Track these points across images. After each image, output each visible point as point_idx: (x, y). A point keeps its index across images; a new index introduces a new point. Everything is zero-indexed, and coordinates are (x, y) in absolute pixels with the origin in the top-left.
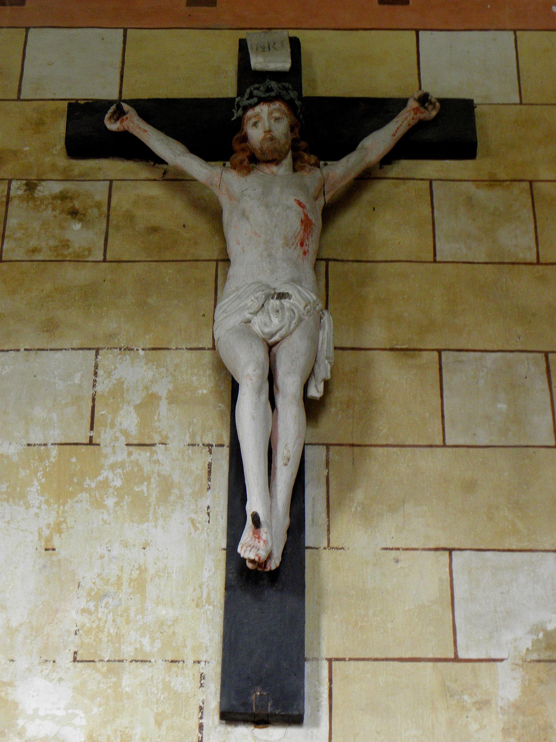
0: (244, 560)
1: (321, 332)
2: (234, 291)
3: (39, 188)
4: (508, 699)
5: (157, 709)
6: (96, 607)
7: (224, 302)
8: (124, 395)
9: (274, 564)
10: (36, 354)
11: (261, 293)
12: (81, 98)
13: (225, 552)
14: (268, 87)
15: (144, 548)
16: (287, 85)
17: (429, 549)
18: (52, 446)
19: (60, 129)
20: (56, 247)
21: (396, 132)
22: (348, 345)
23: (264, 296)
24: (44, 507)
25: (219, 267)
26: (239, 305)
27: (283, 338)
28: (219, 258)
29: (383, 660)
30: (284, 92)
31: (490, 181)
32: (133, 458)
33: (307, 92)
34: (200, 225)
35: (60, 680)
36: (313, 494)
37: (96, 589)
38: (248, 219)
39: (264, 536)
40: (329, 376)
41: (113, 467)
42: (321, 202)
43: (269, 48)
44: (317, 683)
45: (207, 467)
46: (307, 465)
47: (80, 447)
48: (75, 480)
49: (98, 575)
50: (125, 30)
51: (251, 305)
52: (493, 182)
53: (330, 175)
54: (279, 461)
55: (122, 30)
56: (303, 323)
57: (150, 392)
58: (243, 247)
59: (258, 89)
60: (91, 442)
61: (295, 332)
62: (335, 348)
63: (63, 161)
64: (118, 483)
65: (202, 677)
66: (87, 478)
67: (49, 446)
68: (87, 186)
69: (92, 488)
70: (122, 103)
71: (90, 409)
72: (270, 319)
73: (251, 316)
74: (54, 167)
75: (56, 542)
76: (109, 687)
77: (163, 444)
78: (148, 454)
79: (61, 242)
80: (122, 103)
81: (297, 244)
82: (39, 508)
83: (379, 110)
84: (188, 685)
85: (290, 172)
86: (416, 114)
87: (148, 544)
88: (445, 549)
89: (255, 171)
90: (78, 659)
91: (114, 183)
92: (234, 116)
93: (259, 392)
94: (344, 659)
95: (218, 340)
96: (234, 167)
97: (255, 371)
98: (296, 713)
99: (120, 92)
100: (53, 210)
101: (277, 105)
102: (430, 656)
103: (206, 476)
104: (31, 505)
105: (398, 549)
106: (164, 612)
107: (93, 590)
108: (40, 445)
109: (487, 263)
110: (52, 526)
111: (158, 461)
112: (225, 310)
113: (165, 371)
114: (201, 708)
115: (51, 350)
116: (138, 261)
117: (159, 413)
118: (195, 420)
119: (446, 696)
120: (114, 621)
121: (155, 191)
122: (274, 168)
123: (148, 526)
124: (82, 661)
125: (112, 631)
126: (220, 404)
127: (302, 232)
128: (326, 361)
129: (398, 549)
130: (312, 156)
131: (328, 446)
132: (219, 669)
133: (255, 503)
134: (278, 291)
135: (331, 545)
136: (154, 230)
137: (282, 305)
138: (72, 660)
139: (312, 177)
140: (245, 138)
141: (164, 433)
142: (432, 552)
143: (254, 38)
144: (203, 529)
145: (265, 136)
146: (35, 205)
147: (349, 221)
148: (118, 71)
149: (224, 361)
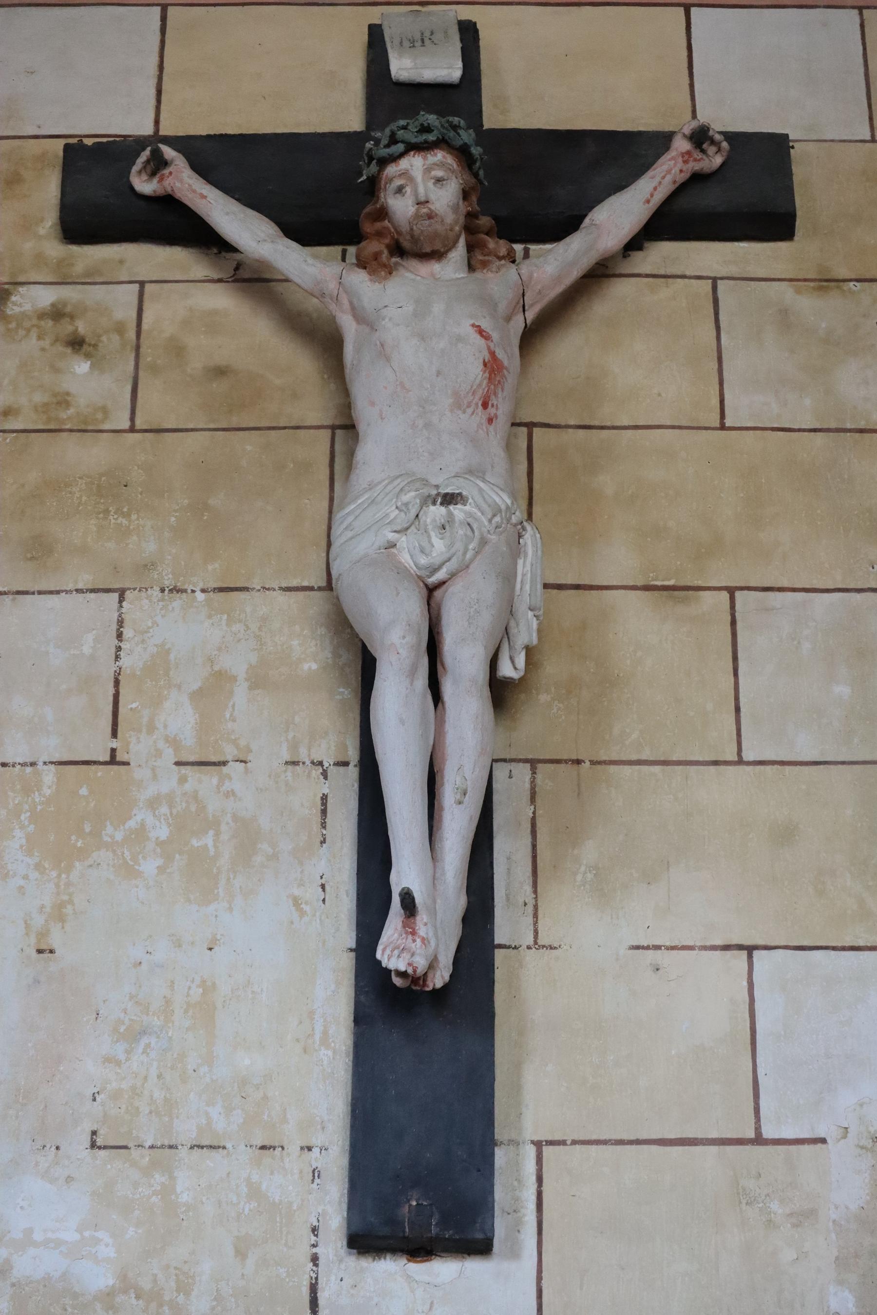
0: (388, 972)
1: (520, 562)
2: (366, 490)
3: (13, 298)
4: (847, 1208)
5: (239, 1231)
6: (128, 1052)
7: (347, 510)
8: (171, 673)
9: (440, 979)
10: (14, 600)
11: (413, 494)
12: (87, 133)
13: (353, 955)
14: (422, 125)
15: (210, 949)
16: (456, 120)
17: (714, 948)
18: (45, 767)
19: (47, 192)
20: (46, 405)
21: (652, 195)
22: (570, 581)
23: (418, 501)
24: (34, 875)
25: (337, 439)
26: (375, 515)
27: (453, 575)
28: (337, 423)
29: (631, 1142)
30: (452, 134)
31: (821, 280)
32: (188, 787)
33: (491, 120)
34: (300, 363)
35: (69, 1179)
36: (509, 851)
37: (127, 1021)
38: (388, 359)
39: (422, 931)
40: (535, 641)
41: (153, 804)
42: (518, 325)
43: (423, 41)
44: (516, 1183)
45: (319, 802)
46: (496, 798)
47: (93, 767)
48: (87, 828)
49: (132, 997)
50: (164, 8)
51: (395, 518)
52: (826, 282)
53: (535, 275)
54: (448, 795)
55: (158, 9)
56: (487, 547)
57: (217, 668)
58: (381, 411)
59: (405, 128)
60: (113, 760)
61: (476, 562)
62: (546, 586)
63: (56, 249)
64: (163, 833)
65: (316, 1174)
66: (108, 823)
67: (40, 766)
68: (98, 293)
69: (117, 842)
70: (161, 146)
71: (111, 699)
72: (430, 541)
73: (396, 535)
74: (39, 260)
75: (55, 940)
76: (155, 1193)
77: (241, 761)
78: (215, 781)
79: (55, 395)
80: (161, 146)
81: (477, 404)
82: (26, 877)
83: (619, 154)
84: (291, 1188)
85: (462, 274)
86: (685, 162)
87: (217, 940)
88: (740, 947)
89: (402, 271)
90: (98, 1144)
91: (148, 287)
92: (362, 175)
93: (412, 674)
94: (563, 1143)
95: (338, 580)
96: (362, 264)
97: (404, 637)
98: (479, 1236)
99: (157, 122)
100: (39, 338)
101: (439, 156)
102: (714, 1135)
103: (318, 818)
104: (11, 873)
105: (657, 948)
106: (247, 1062)
107: (123, 1024)
108: (23, 765)
109: (815, 430)
110: (48, 910)
111: (233, 793)
112: (350, 524)
113: (242, 631)
114: (314, 1230)
115: (40, 593)
116: (192, 430)
117: (233, 706)
118: (297, 719)
119: (740, 1202)
120: (159, 1076)
121: (221, 300)
122: (436, 267)
123: (216, 910)
124: (105, 1147)
125: (156, 1095)
126: (341, 690)
127: (485, 382)
128: (530, 614)
129: (657, 948)
130: (502, 242)
131: (534, 763)
132: (345, 1161)
133: (407, 872)
134: (443, 491)
135: (540, 942)
136: (220, 372)
137: (450, 515)
138: (88, 1144)
139: (501, 281)
140: (383, 213)
141: (242, 743)
142: (718, 953)
143: (396, 20)
144: (314, 915)
145: (417, 210)
146: (8, 330)
147: (569, 351)
148: (153, 82)
149: (350, 617)
